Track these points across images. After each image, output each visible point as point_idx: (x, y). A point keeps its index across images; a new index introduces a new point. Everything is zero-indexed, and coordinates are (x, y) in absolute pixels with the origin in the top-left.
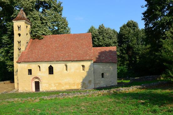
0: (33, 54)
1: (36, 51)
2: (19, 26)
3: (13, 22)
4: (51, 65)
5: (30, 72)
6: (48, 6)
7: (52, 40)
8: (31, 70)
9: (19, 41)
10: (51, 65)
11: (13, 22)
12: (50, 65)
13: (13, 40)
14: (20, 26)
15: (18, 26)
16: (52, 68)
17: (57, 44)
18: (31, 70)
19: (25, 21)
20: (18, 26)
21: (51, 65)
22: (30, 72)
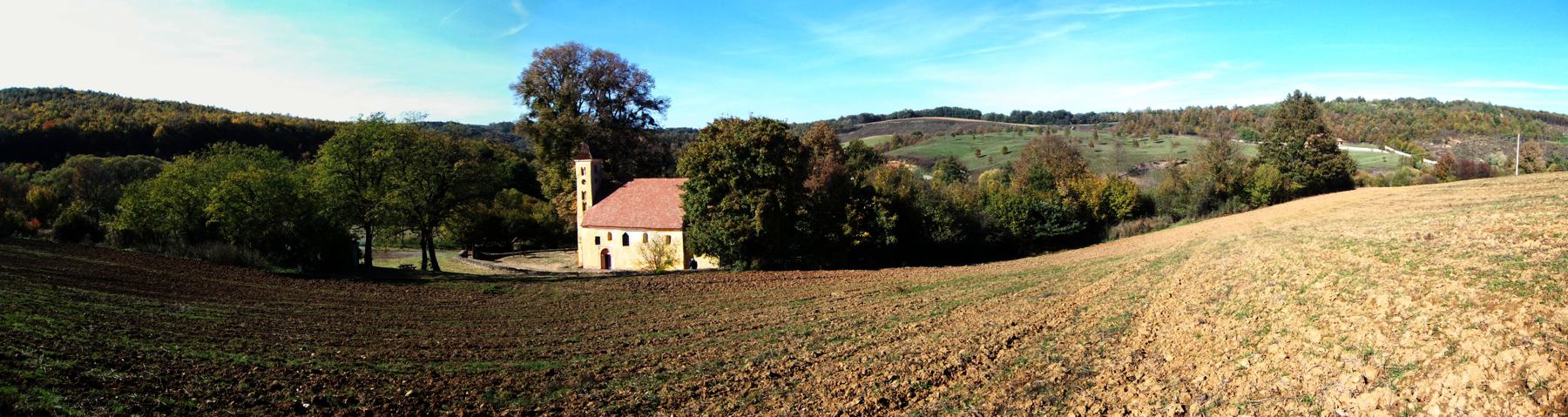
1: (608, 209)
5: (598, 240)
12: (624, 232)
22: (598, 240)
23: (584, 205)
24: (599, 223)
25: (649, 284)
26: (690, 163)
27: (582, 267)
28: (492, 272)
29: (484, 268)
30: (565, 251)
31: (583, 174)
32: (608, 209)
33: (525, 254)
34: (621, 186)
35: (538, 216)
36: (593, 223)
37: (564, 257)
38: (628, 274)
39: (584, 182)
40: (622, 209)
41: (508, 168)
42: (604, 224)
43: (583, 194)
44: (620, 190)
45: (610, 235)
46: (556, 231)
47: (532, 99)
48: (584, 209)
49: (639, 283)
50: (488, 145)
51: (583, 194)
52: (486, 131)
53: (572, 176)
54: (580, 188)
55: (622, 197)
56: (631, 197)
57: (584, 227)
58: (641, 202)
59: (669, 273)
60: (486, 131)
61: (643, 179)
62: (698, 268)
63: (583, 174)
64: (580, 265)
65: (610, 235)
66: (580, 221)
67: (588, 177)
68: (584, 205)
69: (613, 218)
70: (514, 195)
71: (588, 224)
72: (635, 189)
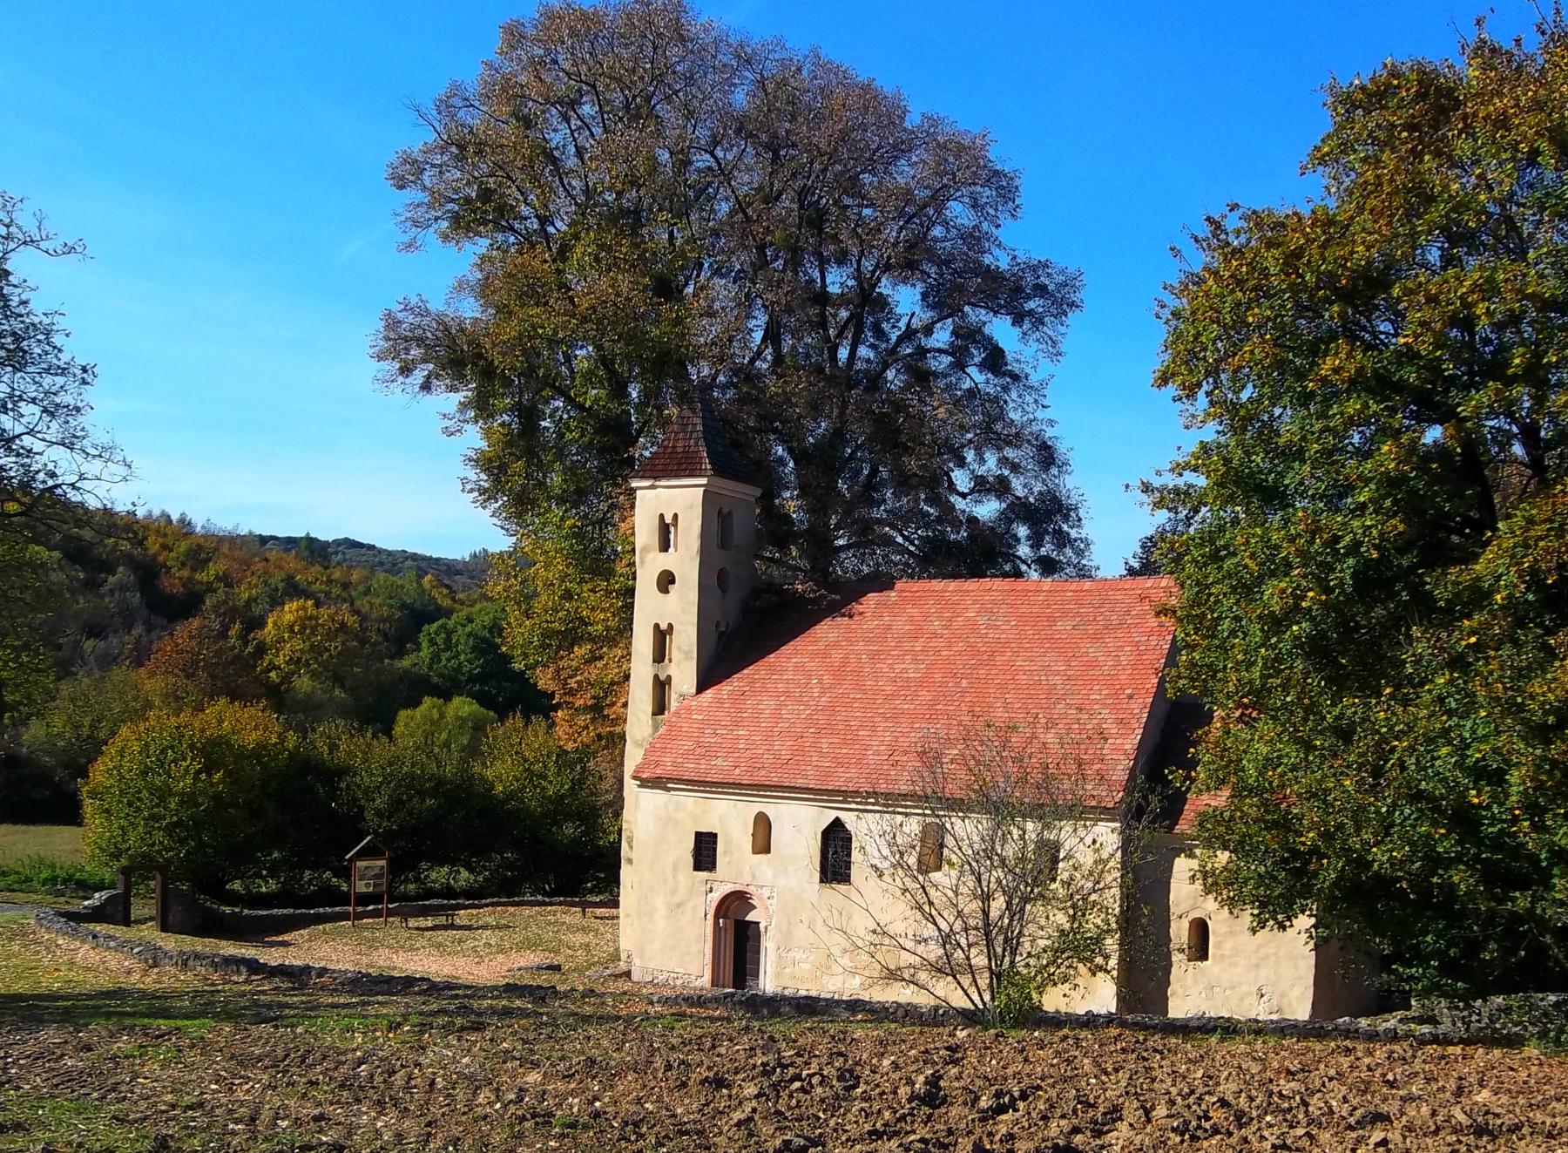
0: (737, 723)
1: (768, 705)
2: (668, 520)
3: (634, 490)
4: (837, 819)
5: (705, 851)
6: (925, 501)
7: (889, 628)
8: (712, 837)
9: (664, 626)
10: (837, 819)
11: (634, 490)
12: (833, 815)
13: (630, 621)
14: (676, 516)
15: (662, 516)
16: (848, 839)
17: (915, 660)
18: (712, 837)
19: (704, 481)
20: (662, 516)
21: (843, 816)
22: (705, 851)
23: (661, 687)
24: (720, 767)
25: (933, 1097)
26: (1263, 292)
27: (628, 974)
28: (150, 982)
29: (114, 960)
30: (584, 905)
31: (665, 546)
32: (768, 705)
33: (405, 915)
34: (834, 609)
35: (500, 773)
36: (690, 769)
37: (573, 929)
38: (808, 1007)
39: (666, 581)
40: (831, 709)
41: (460, 634)
42: (737, 775)
43: (662, 636)
44: (827, 631)
45: (763, 825)
46: (569, 830)
47: (541, 372)
48: (660, 707)
49: (849, 1077)
50: (435, 593)
51: (662, 636)
52: (459, 573)
53: (620, 568)
54: (649, 608)
55: (836, 656)
56: (874, 656)
57: (645, 783)
58: (921, 683)
59: (1057, 1022)
60: (459, 573)
61: (937, 584)
62: (1169, 1016)
63: (665, 546)
64: (623, 966)
65: (763, 825)
66: (633, 757)
67: (685, 559)
68: (661, 687)
69: (784, 747)
70: (463, 720)
71: (667, 768)
72: (901, 625)
